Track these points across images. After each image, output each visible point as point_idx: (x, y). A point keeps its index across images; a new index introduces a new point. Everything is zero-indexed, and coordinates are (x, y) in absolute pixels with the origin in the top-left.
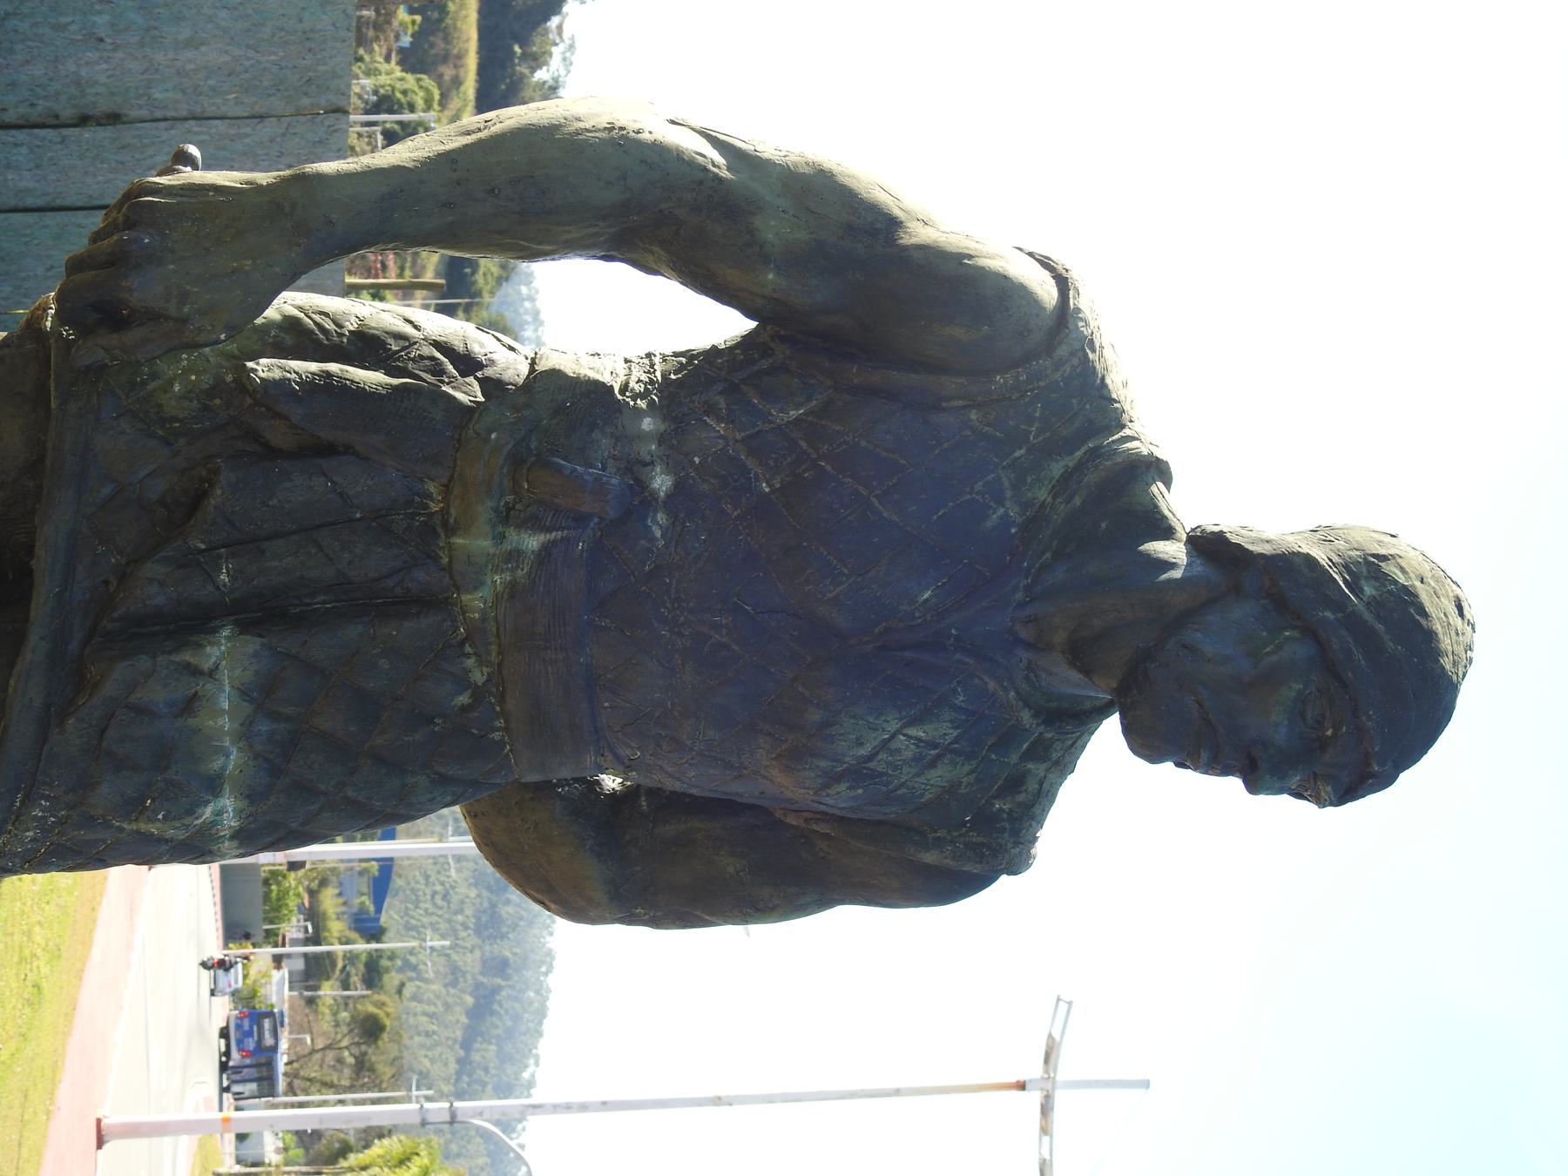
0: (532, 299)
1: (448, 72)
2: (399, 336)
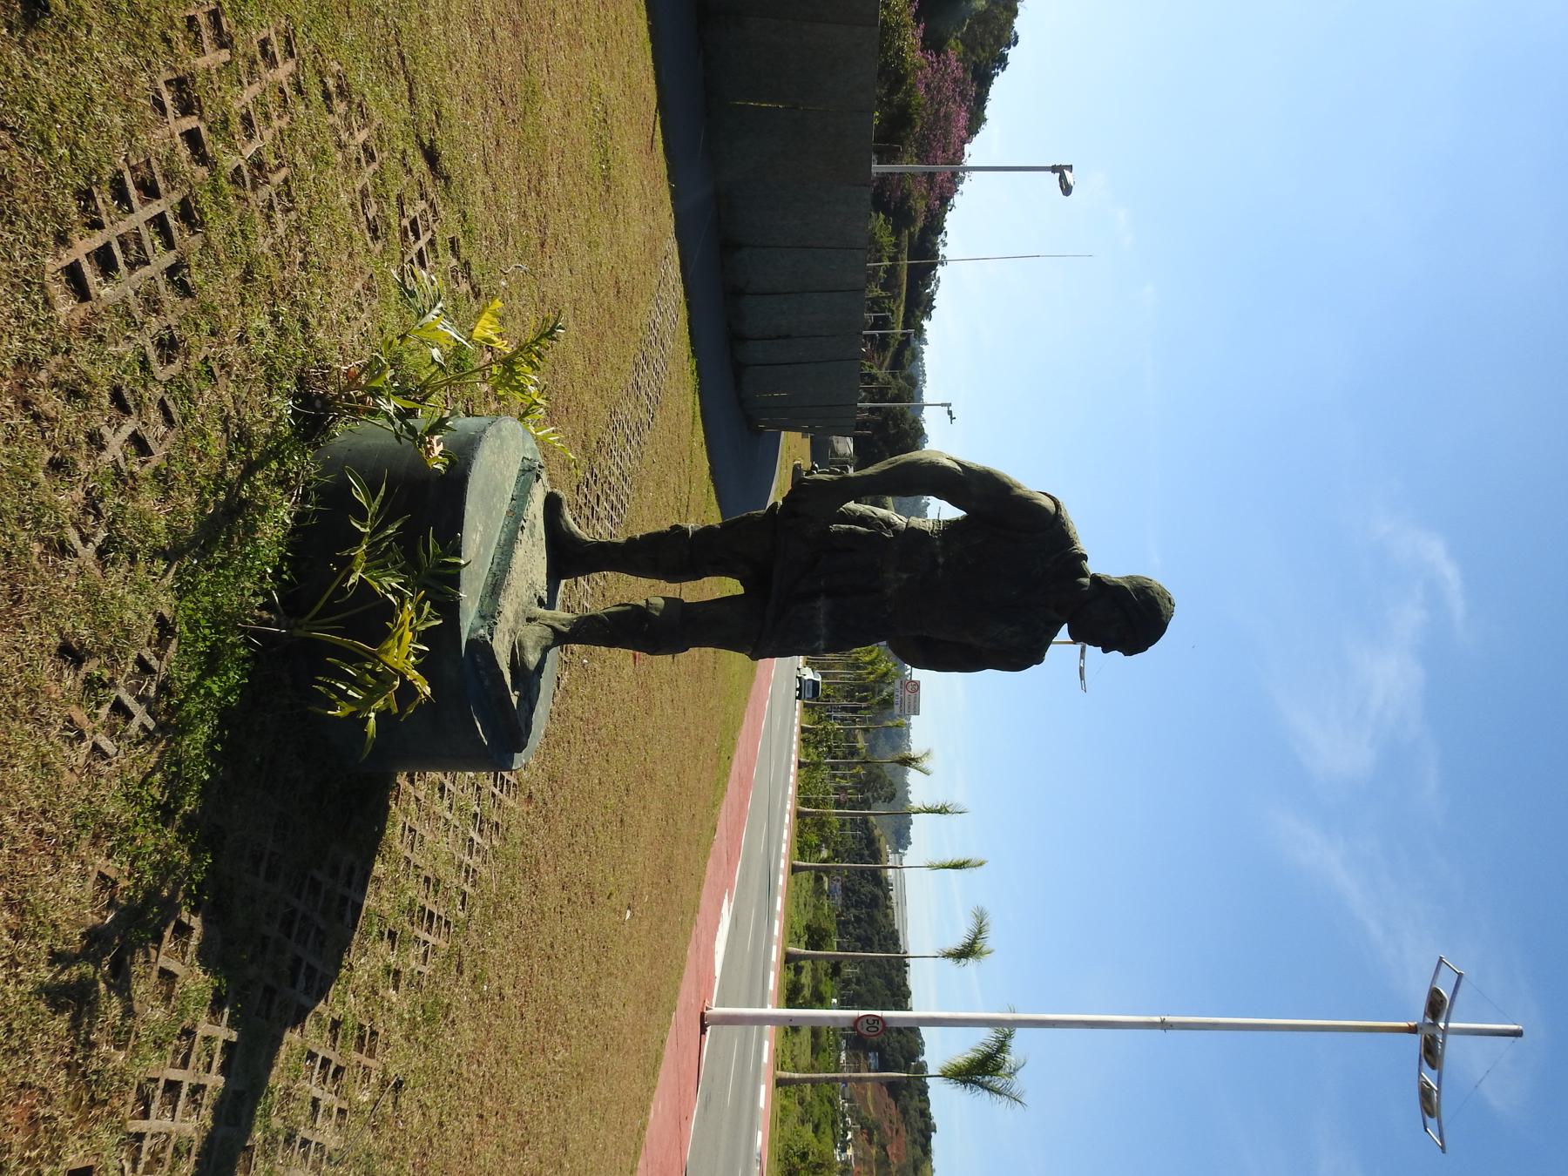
0: (923, 367)
1: (896, 291)
2: (871, 517)
